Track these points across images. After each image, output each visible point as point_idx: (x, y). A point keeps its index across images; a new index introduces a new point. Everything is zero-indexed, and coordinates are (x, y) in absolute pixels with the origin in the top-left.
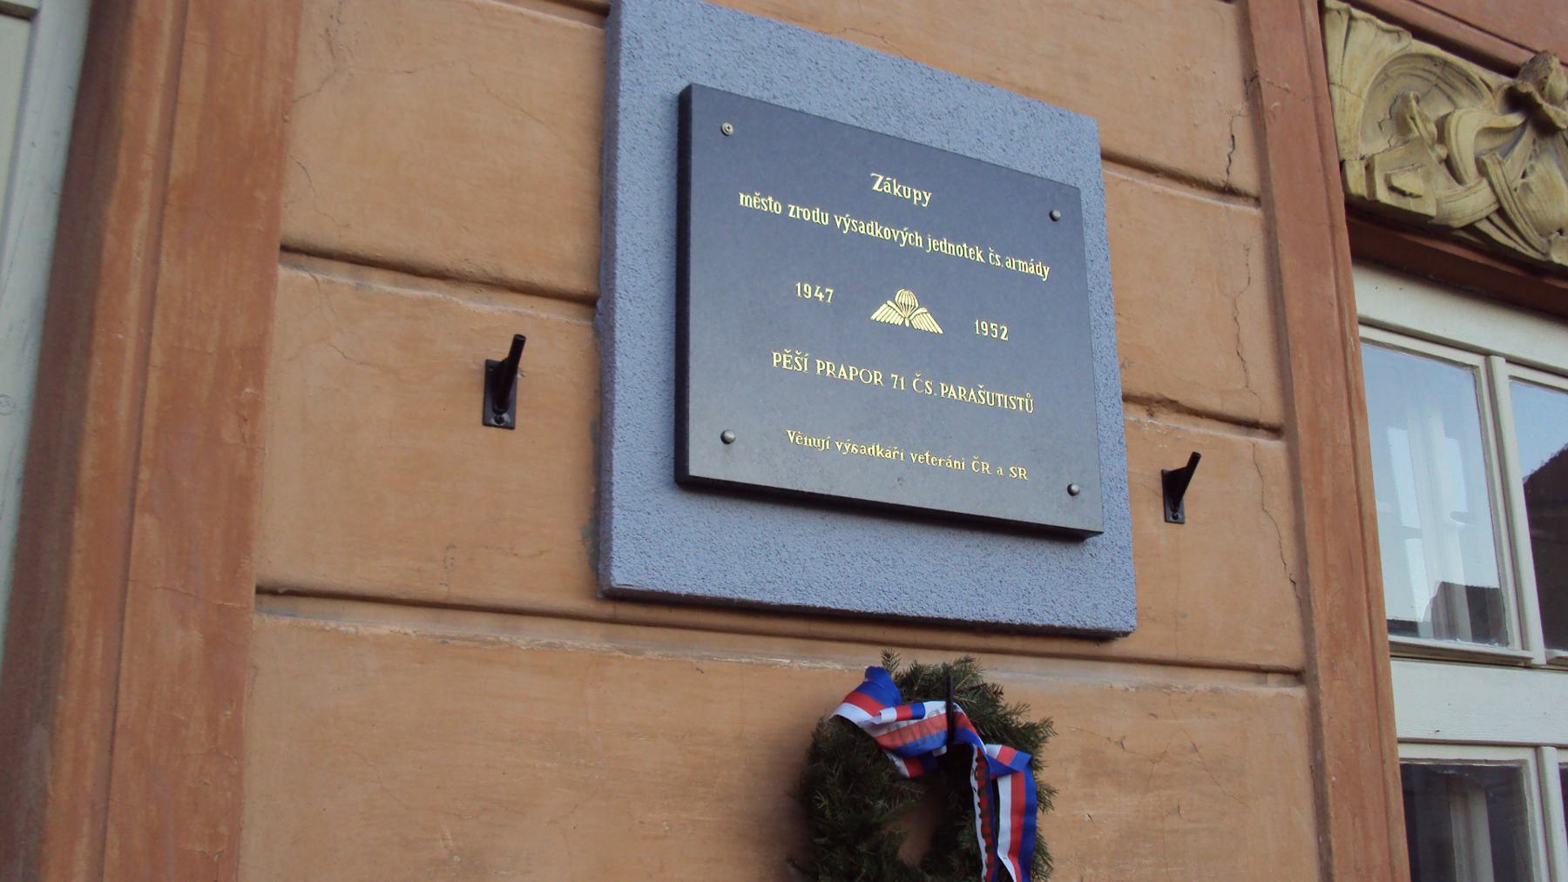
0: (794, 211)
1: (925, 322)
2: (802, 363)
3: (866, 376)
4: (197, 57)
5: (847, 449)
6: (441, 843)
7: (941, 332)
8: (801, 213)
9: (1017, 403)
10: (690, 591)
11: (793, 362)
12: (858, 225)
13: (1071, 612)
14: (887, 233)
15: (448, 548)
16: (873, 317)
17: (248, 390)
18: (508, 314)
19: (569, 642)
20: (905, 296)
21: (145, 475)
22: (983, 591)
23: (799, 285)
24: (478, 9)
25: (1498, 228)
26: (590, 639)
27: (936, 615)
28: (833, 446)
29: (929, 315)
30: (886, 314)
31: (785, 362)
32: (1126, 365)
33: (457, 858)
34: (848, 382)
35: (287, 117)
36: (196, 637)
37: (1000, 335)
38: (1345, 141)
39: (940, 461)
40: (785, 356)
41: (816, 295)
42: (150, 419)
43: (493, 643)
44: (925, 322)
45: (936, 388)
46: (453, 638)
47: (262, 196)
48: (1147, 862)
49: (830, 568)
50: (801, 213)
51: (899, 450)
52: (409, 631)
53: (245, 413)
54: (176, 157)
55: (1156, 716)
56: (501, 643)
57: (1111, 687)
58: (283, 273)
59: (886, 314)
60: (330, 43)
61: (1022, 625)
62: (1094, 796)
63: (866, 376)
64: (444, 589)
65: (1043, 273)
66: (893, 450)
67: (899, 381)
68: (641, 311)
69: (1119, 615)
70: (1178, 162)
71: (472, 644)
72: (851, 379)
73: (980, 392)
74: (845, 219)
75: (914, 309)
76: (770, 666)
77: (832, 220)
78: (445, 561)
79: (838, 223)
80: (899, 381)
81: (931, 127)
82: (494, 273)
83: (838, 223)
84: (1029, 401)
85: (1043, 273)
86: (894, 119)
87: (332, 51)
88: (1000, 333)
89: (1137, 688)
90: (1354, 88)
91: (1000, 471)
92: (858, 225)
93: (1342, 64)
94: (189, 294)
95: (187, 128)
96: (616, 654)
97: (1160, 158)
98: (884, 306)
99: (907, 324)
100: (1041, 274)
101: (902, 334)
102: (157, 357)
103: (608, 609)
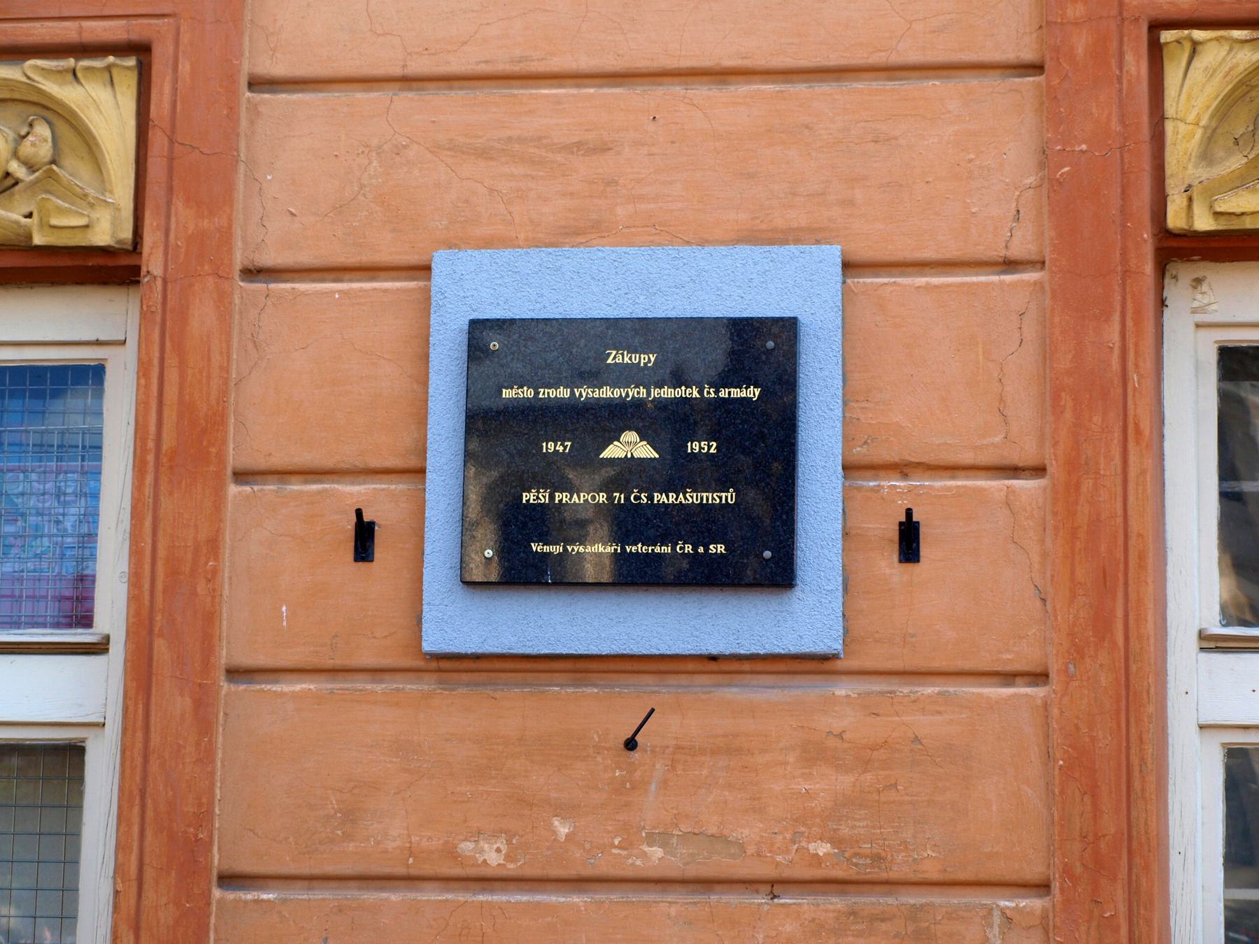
0: (528, 393)
1: (645, 451)
2: (544, 497)
3: (594, 498)
4: (172, 375)
5: (576, 550)
6: (330, 806)
7: (657, 456)
8: (548, 393)
9: (721, 498)
10: (474, 651)
11: (538, 498)
12: (593, 392)
13: (775, 643)
14: (617, 393)
15: (334, 637)
16: (601, 456)
17: (211, 563)
18: (355, 492)
19: (409, 686)
20: (630, 436)
21: (159, 618)
22: (698, 633)
23: (544, 444)
24: (346, 293)
25: (52, 634)
26: (425, 685)
27: (657, 652)
28: (565, 550)
29: (648, 446)
30: (613, 451)
31: (532, 498)
32: (869, 441)
33: (339, 815)
34: (580, 504)
35: (225, 399)
36: (188, 701)
37: (709, 449)
38: (1172, 175)
39: (650, 548)
40: (532, 494)
41: (557, 448)
42: (160, 586)
43: (361, 690)
44: (645, 451)
45: (650, 498)
46: (338, 690)
47: (213, 450)
48: (861, 824)
49: (574, 628)
50: (548, 393)
51: (617, 545)
52: (312, 687)
53: (209, 576)
54: (165, 435)
55: (877, 715)
56: (367, 690)
57: (834, 694)
58: (233, 489)
59: (613, 451)
60: (255, 342)
61: (730, 655)
62: (810, 774)
63: (594, 498)
64: (332, 661)
65: (754, 394)
66: (611, 546)
67: (620, 498)
68: (443, 478)
69: (823, 641)
70: (952, 251)
71: (347, 692)
72: (582, 502)
73: (687, 495)
74: (583, 390)
75: (636, 443)
76: (544, 692)
77: (573, 393)
78: (332, 645)
79: (577, 394)
80: (620, 498)
81: (675, 296)
82: (361, 466)
83: (577, 394)
84: (732, 495)
85: (754, 394)
86: (642, 298)
87: (256, 346)
88: (709, 447)
89: (859, 694)
90: (1191, 118)
91: (701, 550)
92: (593, 392)
93: (1179, 95)
94: (177, 515)
95: (170, 416)
96: (438, 691)
97: (928, 254)
98: (611, 446)
99: (629, 456)
100: (752, 396)
101: (630, 465)
102: (162, 553)
103: (434, 665)
